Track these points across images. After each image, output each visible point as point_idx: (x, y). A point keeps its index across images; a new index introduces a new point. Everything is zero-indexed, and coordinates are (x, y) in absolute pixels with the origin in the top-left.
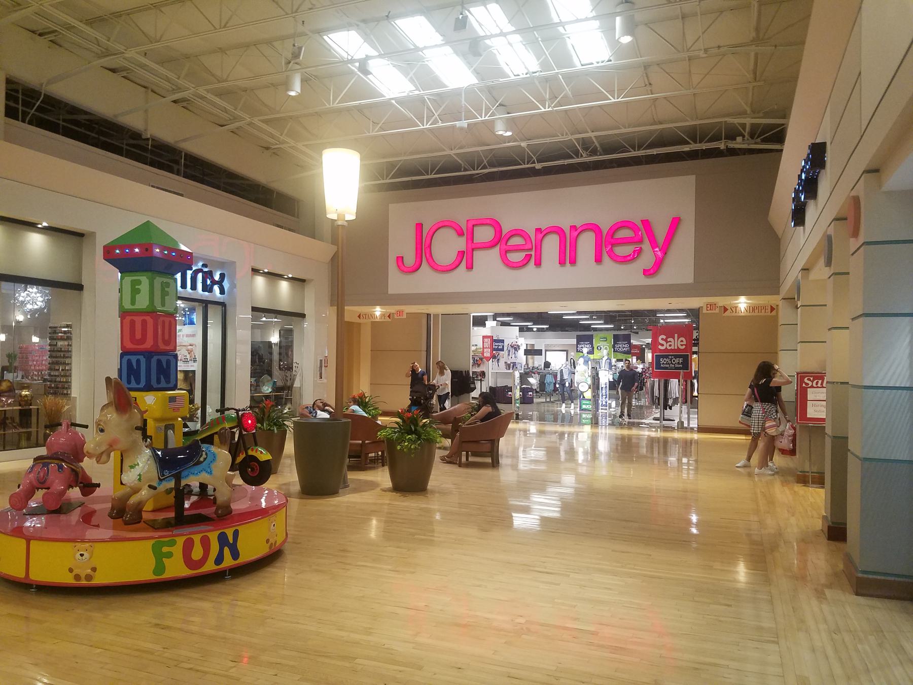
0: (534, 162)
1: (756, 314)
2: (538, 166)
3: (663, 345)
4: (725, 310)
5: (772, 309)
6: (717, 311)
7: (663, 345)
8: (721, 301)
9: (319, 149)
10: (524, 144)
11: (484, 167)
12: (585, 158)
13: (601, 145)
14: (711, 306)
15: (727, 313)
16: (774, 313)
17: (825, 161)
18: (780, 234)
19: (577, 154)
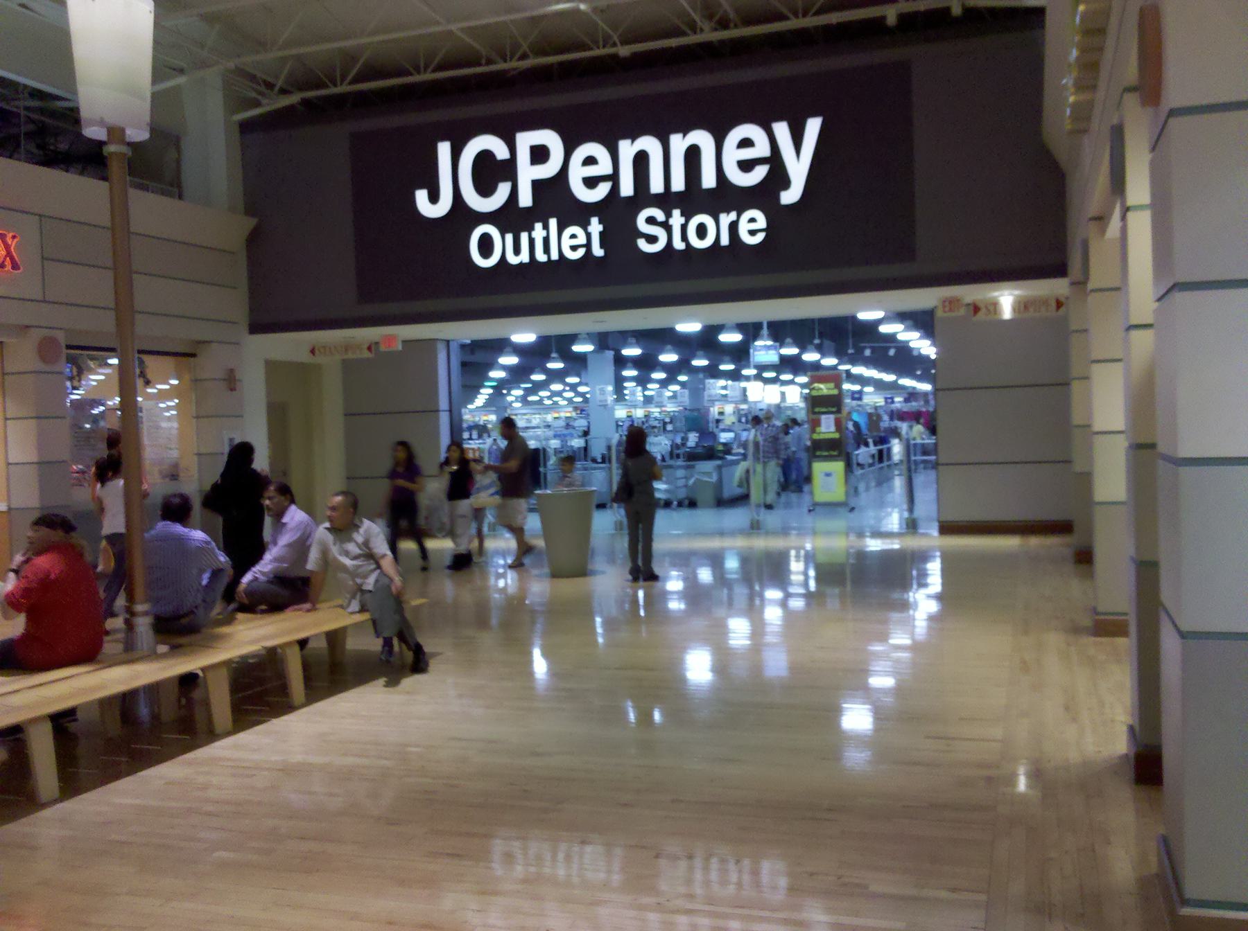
0: (614, 45)
1: (1031, 313)
2: (624, 51)
3: (652, 239)
4: (976, 309)
5: (1059, 305)
6: (962, 311)
7: (652, 239)
8: (970, 293)
9: (684, 649)
10: (453, 27)
11: (524, 57)
12: (709, 35)
13: (737, 11)
14: (951, 303)
15: (981, 315)
16: (1062, 310)
17: (839, 24)
18: (1062, 155)
19: (694, 28)
